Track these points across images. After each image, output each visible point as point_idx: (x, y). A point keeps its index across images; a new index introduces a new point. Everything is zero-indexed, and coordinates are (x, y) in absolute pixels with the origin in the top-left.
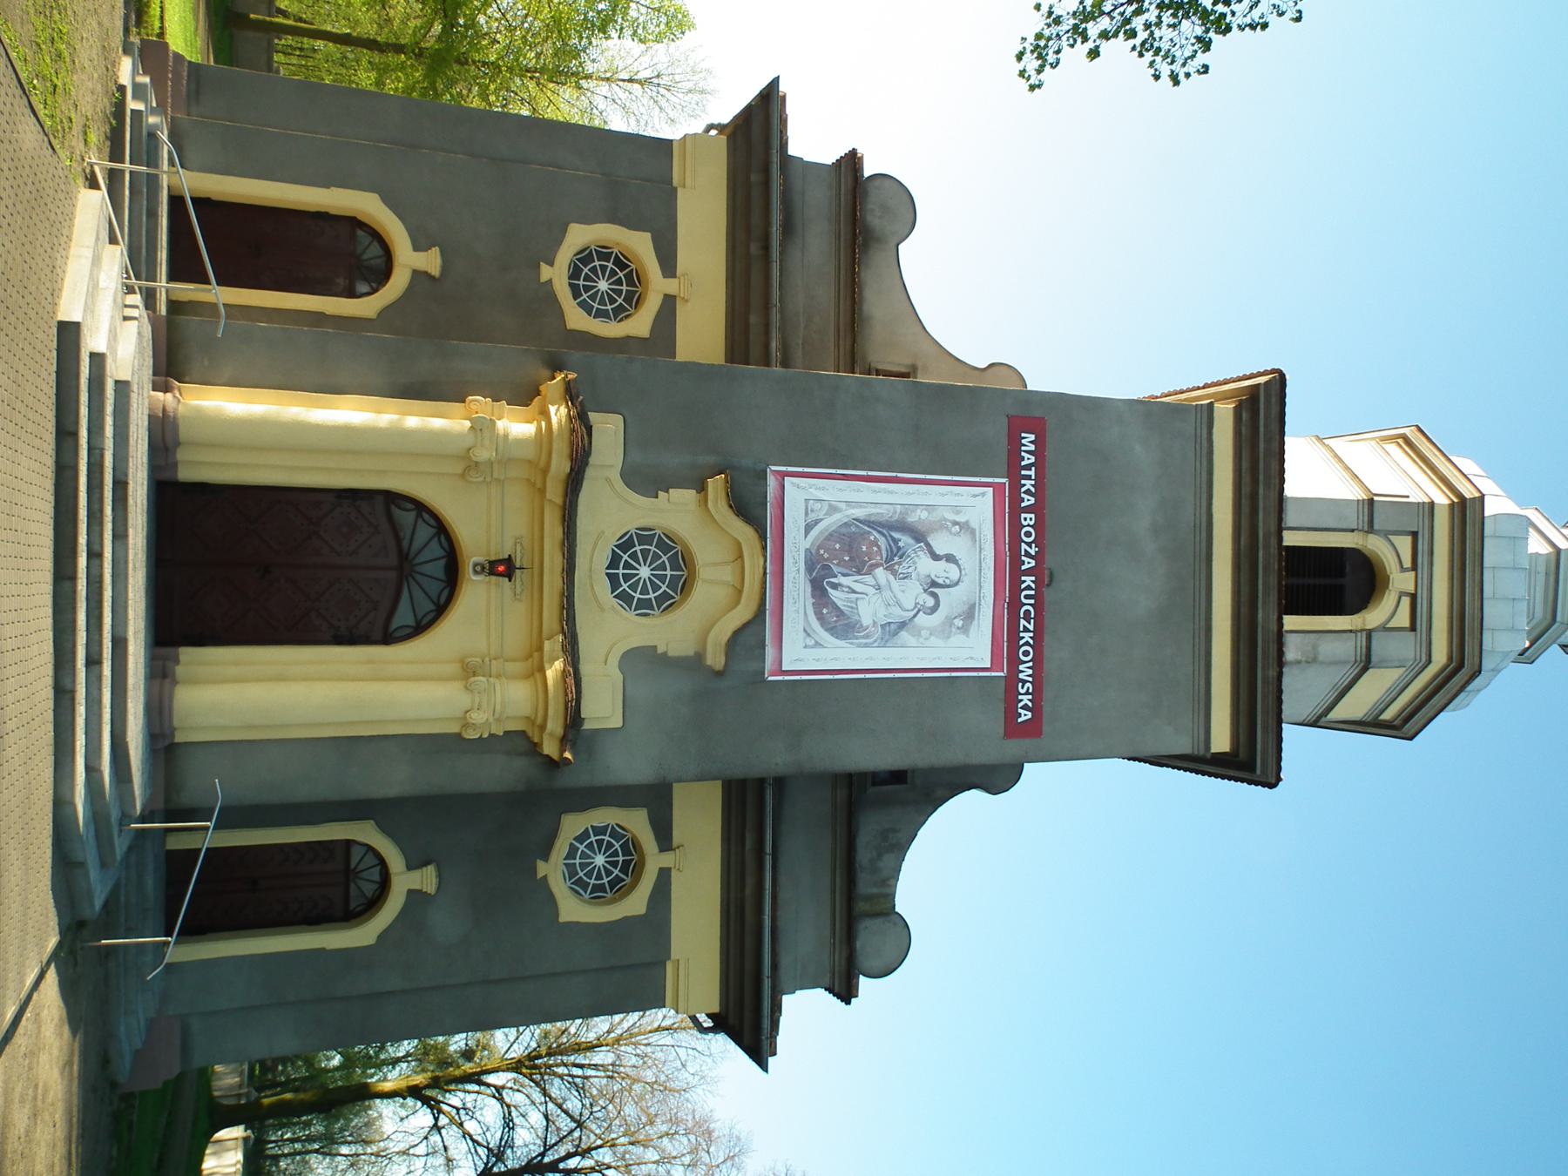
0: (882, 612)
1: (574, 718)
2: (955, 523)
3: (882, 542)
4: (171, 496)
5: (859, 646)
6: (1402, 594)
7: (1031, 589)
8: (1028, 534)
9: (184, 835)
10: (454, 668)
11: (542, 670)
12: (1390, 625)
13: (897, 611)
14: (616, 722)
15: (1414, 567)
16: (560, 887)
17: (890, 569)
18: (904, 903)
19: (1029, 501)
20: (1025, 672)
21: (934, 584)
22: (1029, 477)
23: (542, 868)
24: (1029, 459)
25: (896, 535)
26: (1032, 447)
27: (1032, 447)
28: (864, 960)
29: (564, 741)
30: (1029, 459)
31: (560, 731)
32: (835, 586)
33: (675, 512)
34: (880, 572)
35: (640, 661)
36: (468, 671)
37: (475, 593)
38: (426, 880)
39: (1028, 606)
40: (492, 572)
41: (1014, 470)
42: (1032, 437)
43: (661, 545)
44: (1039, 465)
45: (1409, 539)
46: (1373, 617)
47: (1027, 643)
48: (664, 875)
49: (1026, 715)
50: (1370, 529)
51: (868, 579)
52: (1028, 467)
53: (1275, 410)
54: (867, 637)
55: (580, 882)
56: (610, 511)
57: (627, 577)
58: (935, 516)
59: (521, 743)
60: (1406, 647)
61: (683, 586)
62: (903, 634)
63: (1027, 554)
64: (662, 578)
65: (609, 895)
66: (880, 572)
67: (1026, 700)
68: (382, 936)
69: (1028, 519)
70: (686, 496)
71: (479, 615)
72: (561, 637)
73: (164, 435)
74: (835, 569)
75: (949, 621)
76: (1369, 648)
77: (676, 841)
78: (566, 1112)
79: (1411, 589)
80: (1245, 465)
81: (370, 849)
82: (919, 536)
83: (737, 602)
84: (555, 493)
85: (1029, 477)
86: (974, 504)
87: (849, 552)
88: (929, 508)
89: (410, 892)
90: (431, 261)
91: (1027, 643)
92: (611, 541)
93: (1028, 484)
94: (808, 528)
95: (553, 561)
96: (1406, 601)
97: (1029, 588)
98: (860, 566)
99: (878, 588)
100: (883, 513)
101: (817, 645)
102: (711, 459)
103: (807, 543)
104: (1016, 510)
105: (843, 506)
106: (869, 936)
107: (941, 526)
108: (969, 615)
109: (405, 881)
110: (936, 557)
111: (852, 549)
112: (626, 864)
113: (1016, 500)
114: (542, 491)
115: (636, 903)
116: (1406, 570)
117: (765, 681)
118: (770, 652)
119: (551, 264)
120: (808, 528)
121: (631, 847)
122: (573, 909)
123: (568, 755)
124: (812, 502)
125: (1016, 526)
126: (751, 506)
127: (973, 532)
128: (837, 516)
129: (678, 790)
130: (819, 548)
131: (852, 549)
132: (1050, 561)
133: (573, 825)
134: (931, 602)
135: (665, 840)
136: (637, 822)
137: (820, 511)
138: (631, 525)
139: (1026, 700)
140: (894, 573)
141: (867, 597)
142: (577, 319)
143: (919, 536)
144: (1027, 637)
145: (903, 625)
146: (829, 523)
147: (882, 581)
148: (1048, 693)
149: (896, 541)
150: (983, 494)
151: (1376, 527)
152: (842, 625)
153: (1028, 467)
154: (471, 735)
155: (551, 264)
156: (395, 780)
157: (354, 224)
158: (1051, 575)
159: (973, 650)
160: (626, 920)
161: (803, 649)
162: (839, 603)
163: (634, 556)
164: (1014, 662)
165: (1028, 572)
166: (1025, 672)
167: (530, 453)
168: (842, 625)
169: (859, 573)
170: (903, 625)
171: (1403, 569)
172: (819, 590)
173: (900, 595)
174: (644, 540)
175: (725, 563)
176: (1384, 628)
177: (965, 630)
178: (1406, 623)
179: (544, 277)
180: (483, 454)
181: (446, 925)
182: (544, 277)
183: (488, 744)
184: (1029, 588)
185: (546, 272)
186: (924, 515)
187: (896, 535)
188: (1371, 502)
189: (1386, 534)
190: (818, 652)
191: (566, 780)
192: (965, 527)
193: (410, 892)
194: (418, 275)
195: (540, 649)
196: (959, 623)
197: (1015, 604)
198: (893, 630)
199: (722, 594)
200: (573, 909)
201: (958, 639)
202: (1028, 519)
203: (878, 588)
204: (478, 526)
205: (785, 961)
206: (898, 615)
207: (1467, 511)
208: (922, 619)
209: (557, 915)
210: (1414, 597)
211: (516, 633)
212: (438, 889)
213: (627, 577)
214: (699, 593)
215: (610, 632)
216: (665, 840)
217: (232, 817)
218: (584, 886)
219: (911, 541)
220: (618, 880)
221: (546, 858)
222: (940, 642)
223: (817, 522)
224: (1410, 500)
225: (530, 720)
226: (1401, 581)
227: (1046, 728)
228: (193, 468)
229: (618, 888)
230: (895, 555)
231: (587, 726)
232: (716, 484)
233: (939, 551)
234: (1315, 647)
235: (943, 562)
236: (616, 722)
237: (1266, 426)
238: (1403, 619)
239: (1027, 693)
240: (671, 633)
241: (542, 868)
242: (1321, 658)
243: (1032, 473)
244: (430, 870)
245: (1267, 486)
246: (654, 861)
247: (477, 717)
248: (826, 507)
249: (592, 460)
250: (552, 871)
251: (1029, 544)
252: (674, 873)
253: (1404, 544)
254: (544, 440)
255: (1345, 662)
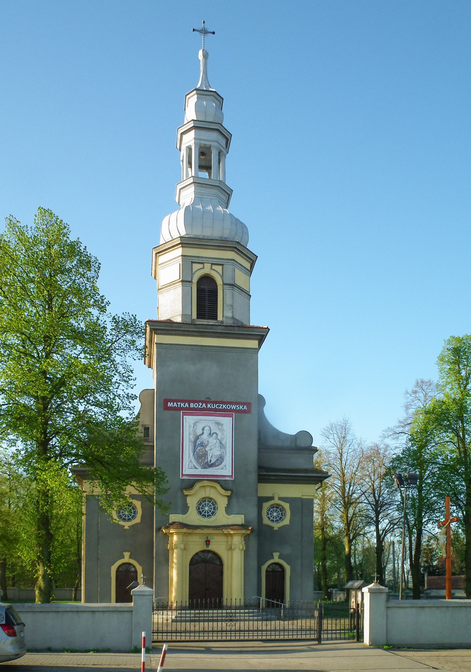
0: (217, 449)
1: (243, 526)
2: (194, 427)
3: (199, 448)
4: (192, 607)
5: (226, 455)
6: (211, 269)
7: (211, 406)
8: (196, 405)
9: (209, 138)
10: (230, 552)
11: (231, 534)
12: (221, 274)
13: (217, 444)
14: (243, 516)
15: (203, 263)
16: (281, 524)
17: (206, 446)
18: (293, 432)
19: (187, 405)
20: (234, 407)
21: (210, 434)
22: (180, 404)
23: (276, 528)
24: (175, 404)
25: (197, 444)
26: (172, 403)
27: (172, 403)
28: (308, 445)
29: (247, 529)
30: (175, 404)
31: (245, 530)
32: (211, 461)
33: (192, 502)
34: (207, 449)
35: (229, 510)
36: (230, 549)
37: (212, 547)
38: (276, 555)
39: (216, 406)
40: (209, 544)
41: (180, 409)
42: (169, 403)
43: (200, 504)
44: (177, 401)
45: (194, 265)
46: (219, 281)
47: (226, 406)
48: (280, 499)
49: (245, 407)
50: (191, 282)
51: (209, 452)
52: (177, 405)
53: (158, 324)
54: (223, 453)
55: (280, 519)
56: (192, 517)
57: (208, 513)
58: (192, 433)
59: (246, 538)
60: (228, 267)
61: (210, 499)
62: (223, 442)
63: (202, 406)
64: (208, 504)
65: (284, 512)
66: (207, 449)
67: (241, 407)
68: (288, 564)
69: (192, 405)
70: (189, 500)
71: (218, 546)
72: (223, 530)
73: (181, 608)
74: (206, 461)
75: (220, 429)
76: (228, 285)
77: (272, 496)
78: (236, 608)
79: (210, 265)
80: (174, 332)
81: (269, 566)
82: (197, 438)
83: (215, 487)
84: (190, 531)
85: (180, 404)
86: (189, 421)
87: (202, 457)
88: (190, 434)
89: (279, 558)
90: (127, 555)
91: (226, 406)
92: (200, 517)
93: (182, 405)
94: (196, 468)
95: (206, 531)
96: (214, 267)
97: (211, 405)
98: (205, 454)
99: (211, 449)
100: (191, 448)
101: (225, 466)
102: (179, 493)
103: (200, 468)
104: (189, 409)
105: (190, 459)
106: (302, 443)
107: (194, 431)
108: (218, 424)
109: (276, 559)
110: (203, 433)
111: (201, 457)
112: (276, 507)
113: (186, 409)
114: (189, 533)
115: (287, 506)
116: (204, 266)
117: (234, 480)
118: (227, 479)
119: (124, 526)
120: (196, 468)
121: (272, 506)
122: (286, 521)
123: (250, 528)
124: (189, 467)
125: (194, 409)
126: (190, 484)
127: (196, 422)
128: (193, 460)
129: (259, 495)
130: (201, 465)
131: (201, 457)
132: (203, 399)
133: (266, 521)
134: (215, 435)
135: (272, 498)
136: (266, 505)
137: (191, 465)
138: (196, 512)
139: (241, 407)
140: (207, 445)
141: (213, 452)
142: (138, 520)
143: (197, 438)
144: (224, 406)
145: (221, 443)
146: (194, 462)
147: (209, 448)
148: (239, 400)
149: (199, 444)
150: (186, 419)
151: (190, 280)
152: (221, 459)
153: (177, 405)
154: (245, 548)
155: (124, 526)
156: (254, 563)
157: (118, 571)
158: (207, 398)
159: (227, 422)
160: (291, 508)
161: (226, 470)
162: (215, 460)
163: (203, 511)
164: (231, 410)
165: (207, 406)
166: (234, 407)
167: (181, 536)
168: (221, 459)
169: (207, 455)
170: (221, 443)
171: (203, 268)
172: (212, 466)
173: (213, 444)
174: (199, 509)
175: (205, 490)
176: (222, 276)
177: (222, 425)
178: (221, 267)
179: (128, 528)
180: (182, 546)
181: (287, 550)
182: (128, 528)
183: (247, 544)
184: (211, 405)
185: (127, 527)
186: (192, 436)
187: (197, 444)
188: (182, 281)
189: (192, 274)
190: (227, 466)
191: (256, 527)
192: (195, 424)
193: (279, 558)
194: (130, 557)
195: (226, 534)
196: (220, 427)
197: (215, 410)
198: (222, 446)
199: (213, 490)
200: (286, 521)
201: (225, 427)
202: (192, 405)
203: (211, 449)
204: (196, 545)
205: (305, 467)
206: (218, 444)
207: (185, 242)
208: (219, 437)
209: (287, 525)
210: (212, 264)
211: (223, 539)
212: (278, 552)
213: (208, 513)
214: (212, 496)
215: (221, 517)
216: (272, 498)
217: (259, 594)
218: (281, 518)
219: (199, 440)
220: (280, 509)
221: (273, 528)
222: (225, 432)
223: (194, 466)
224: (181, 263)
225: (242, 536)
226: (207, 270)
227: (249, 401)
228: (186, 602)
229: (282, 509)
230: (202, 445)
231: (243, 523)
232: (186, 493)
233: (201, 432)
234: (228, 306)
235: (205, 431)
236: (243, 516)
237: (163, 327)
238: (219, 268)
239: (239, 407)
240: (222, 502)
241: (276, 528)
242: (231, 303)
243: (179, 403)
244: (274, 554)
245: (181, 327)
246: (276, 501)
247: (241, 547)
248: (190, 463)
249: (181, 522)
250: (276, 526)
251: (199, 405)
252: (281, 496)
253: (196, 267)
254: (177, 533)
255: (233, 293)
